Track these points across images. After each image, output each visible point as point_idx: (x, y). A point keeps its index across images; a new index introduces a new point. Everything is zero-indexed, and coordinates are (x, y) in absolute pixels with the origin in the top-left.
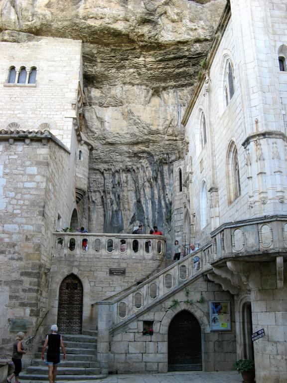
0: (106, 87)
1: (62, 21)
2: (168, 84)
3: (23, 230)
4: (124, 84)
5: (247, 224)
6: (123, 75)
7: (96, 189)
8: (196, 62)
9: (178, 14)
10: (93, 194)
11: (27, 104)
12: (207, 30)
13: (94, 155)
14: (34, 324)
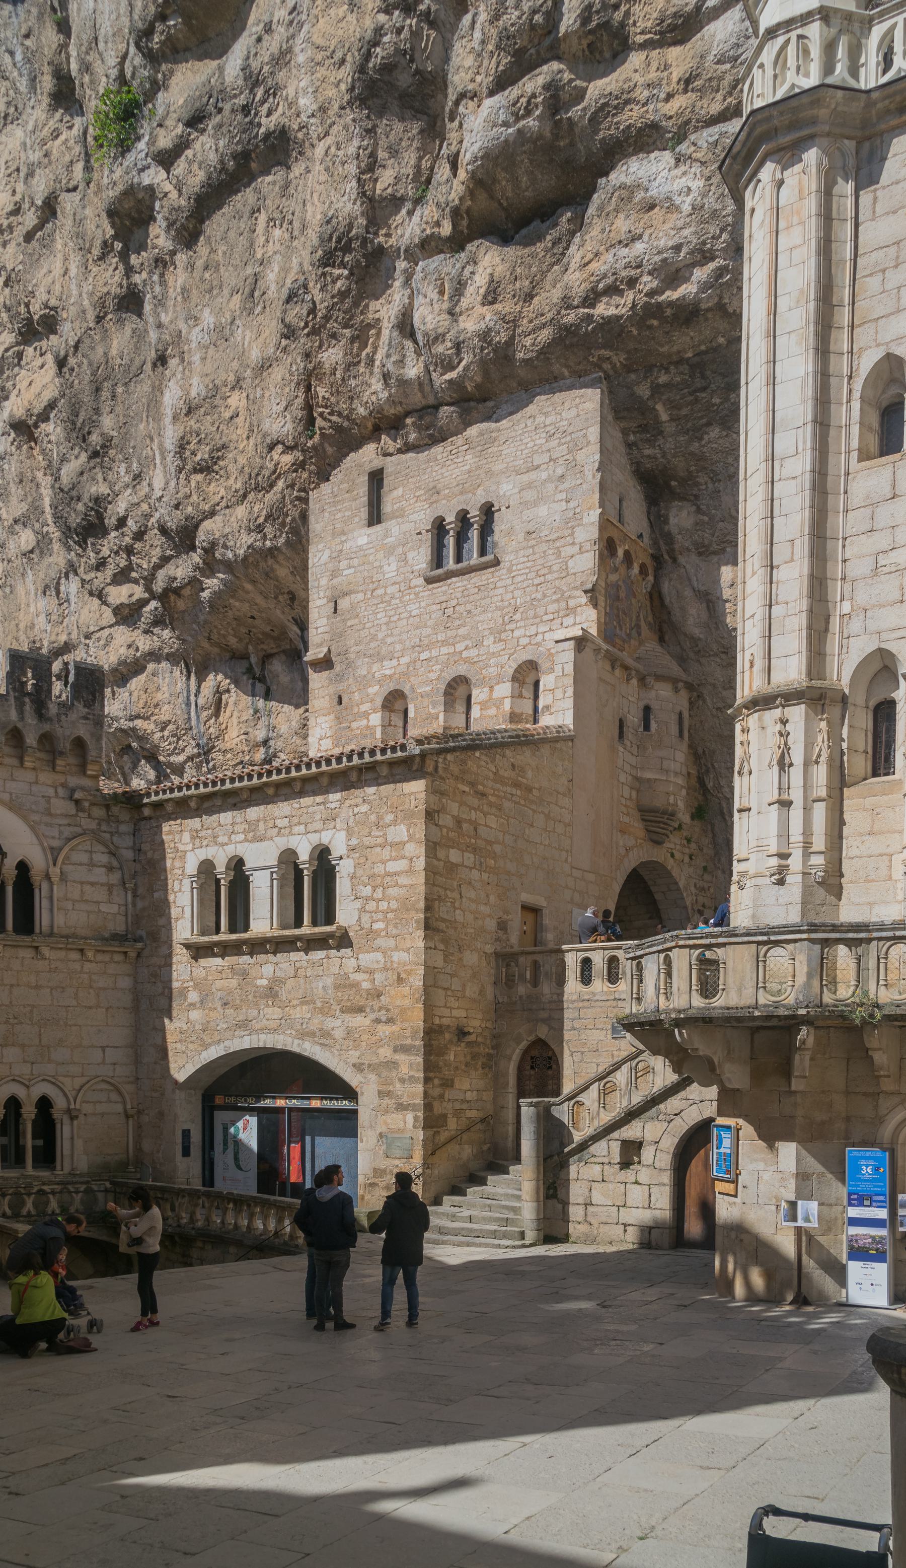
1: (534, 331)
5: (648, 950)
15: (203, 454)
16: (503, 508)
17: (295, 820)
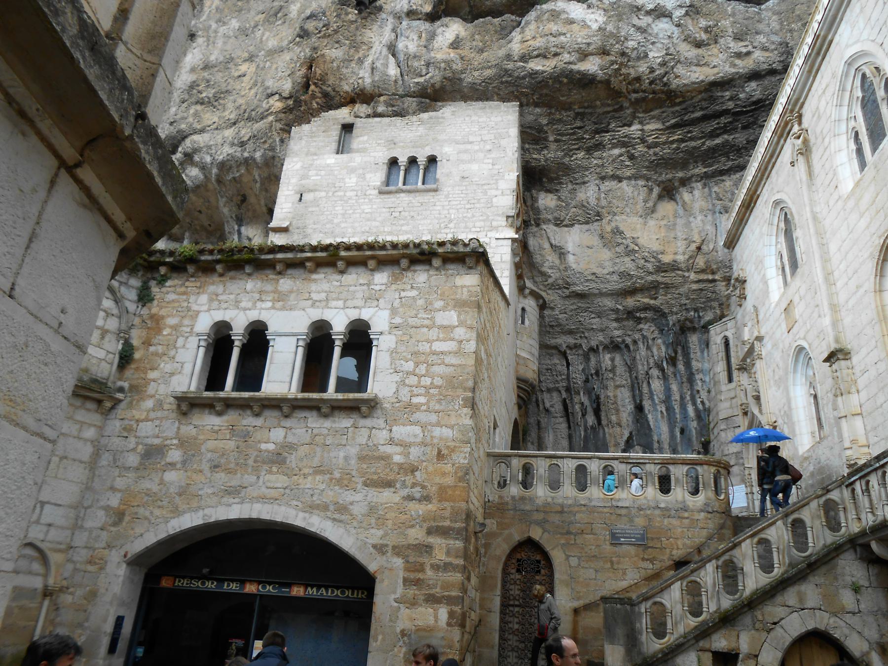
0: (566, 189)
2: (692, 172)
3: (432, 437)
4: (603, 178)
6: (600, 162)
7: (551, 386)
8: (751, 120)
9: (707, 30)
10: (546, 396)
11: (422, 222)
12: (772, 51)
13: (547, 319)
14: (457, 645)
15: (209, 93)
16: (444, 161)
17: (334, 295)
